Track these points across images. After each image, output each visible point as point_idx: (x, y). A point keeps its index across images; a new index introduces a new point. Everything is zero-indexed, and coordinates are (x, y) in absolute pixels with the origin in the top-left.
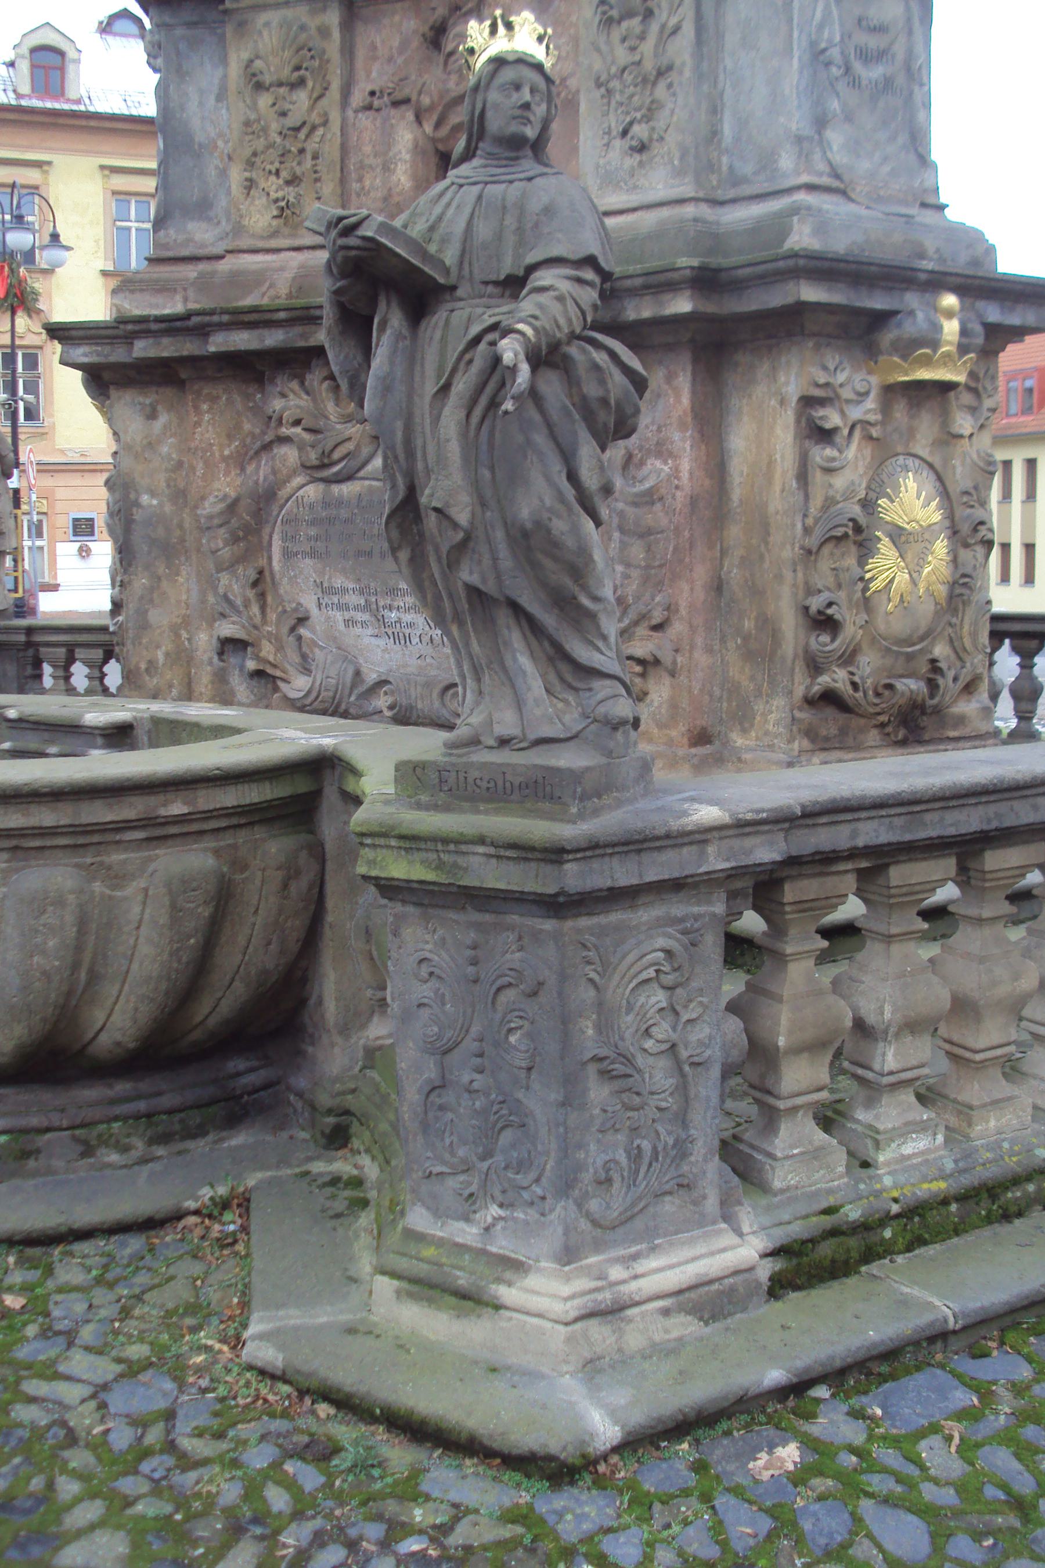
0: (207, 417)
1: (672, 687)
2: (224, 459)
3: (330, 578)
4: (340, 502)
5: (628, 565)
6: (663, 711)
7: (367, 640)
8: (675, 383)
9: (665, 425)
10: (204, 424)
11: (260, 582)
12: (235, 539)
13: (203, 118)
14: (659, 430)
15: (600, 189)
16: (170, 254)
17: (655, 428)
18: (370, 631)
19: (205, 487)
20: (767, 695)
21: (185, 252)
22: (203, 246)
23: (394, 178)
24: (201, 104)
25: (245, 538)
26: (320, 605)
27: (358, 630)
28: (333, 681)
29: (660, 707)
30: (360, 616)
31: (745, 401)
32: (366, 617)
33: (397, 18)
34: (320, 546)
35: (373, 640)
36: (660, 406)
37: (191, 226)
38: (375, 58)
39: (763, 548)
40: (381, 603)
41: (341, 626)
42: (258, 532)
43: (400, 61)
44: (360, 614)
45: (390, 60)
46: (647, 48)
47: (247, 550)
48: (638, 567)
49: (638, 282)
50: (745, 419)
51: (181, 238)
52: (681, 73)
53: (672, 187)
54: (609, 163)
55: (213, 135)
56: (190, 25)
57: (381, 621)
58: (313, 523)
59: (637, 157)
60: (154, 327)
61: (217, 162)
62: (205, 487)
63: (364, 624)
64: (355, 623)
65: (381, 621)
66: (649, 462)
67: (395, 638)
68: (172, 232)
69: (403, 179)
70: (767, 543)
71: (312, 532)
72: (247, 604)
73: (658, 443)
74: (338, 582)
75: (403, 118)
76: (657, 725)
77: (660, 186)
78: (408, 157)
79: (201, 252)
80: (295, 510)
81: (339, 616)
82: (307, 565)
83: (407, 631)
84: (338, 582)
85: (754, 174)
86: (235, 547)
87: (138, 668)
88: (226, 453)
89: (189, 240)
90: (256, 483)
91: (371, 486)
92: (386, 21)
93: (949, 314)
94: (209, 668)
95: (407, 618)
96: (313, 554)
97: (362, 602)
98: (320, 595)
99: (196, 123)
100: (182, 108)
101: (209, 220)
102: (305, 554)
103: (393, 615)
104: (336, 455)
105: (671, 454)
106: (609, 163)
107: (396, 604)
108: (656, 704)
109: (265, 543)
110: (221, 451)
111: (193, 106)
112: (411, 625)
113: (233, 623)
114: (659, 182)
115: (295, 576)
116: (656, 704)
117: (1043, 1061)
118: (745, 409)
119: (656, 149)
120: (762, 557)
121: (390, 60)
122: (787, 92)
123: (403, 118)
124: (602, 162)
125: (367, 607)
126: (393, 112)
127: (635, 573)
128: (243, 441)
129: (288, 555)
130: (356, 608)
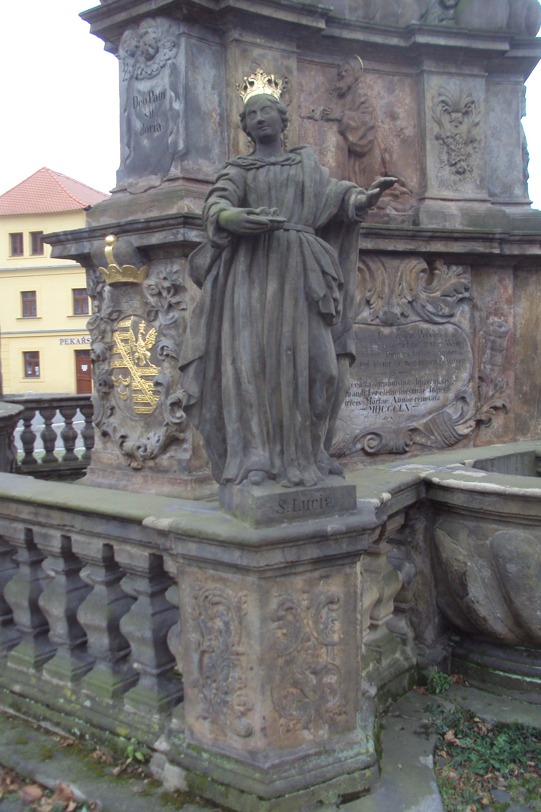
1: (505, 419)
5: (493, 365)
6: (500, 430)
7: (356, 412)
8: (504, 283)
13: (205, 97)
14: (496, 303)
15: (439, 187)
16: (192, 176)
17: (493, 303)
18: (361, 406)
20: (537, 417)
21: (200, 177)
22: (207, 175)
23: (326, 159)
24: (204, 88)
29: (498, 428)
30: (356, 399)
31: (523, 292)
32: (360, 399)
33: (313, 73)
35: (362, 412)
36: (496, 293)
37: (200, 161)
38: (303, 91)
39: (534, 355)
40: (372, 391)
43: (315, 96)
44: (357, 398)
45: (310, 94)
46: (464, 128)
48: (499, 366)
49: (518, 238)
50: (523, 300)
51: (196, 167)
52: (480, 143)
53: (476, 193)
54: (443, 176)
55: (210, 108)
56: (201, 39)
57: (368, 399)
59: (459, 177)
60: (171, 222)
61: (213, 125)
63: (358, 403)
65: (368, 399)
66: (491, 318)
67: (374, 409)
68: (191, 163)
69: (331, 160)
70: (536, 354)
73: (495, 309)
75: (331, 128)
77: (470, 192)
78: (333, 149)
79: (206, 178)
83: (382, 405)
85: (501, 193)
87: (199, 445)
89: (200, 170)
91: (360, 328)
92: (307, 73)
93: (109, 244)
95: (384, 398)
97: (360, 391)
99: (202, 99)
100: (195, 88)
101: (209, 159)
105: (503, 315)
106: (443, 176)
107: (379, 391)
108: (496, 427)
111: (200, 88)
112: (385, 402)
114: (469, 190)
116: (496, 427)
118: (523, 296)
119: (468, 174)
120: (533, 359)
121: (310, 94)
122: (518, 162)
123: (331, 128)
124: (439, 174)
126: (325, 124)
127: (497, 369)
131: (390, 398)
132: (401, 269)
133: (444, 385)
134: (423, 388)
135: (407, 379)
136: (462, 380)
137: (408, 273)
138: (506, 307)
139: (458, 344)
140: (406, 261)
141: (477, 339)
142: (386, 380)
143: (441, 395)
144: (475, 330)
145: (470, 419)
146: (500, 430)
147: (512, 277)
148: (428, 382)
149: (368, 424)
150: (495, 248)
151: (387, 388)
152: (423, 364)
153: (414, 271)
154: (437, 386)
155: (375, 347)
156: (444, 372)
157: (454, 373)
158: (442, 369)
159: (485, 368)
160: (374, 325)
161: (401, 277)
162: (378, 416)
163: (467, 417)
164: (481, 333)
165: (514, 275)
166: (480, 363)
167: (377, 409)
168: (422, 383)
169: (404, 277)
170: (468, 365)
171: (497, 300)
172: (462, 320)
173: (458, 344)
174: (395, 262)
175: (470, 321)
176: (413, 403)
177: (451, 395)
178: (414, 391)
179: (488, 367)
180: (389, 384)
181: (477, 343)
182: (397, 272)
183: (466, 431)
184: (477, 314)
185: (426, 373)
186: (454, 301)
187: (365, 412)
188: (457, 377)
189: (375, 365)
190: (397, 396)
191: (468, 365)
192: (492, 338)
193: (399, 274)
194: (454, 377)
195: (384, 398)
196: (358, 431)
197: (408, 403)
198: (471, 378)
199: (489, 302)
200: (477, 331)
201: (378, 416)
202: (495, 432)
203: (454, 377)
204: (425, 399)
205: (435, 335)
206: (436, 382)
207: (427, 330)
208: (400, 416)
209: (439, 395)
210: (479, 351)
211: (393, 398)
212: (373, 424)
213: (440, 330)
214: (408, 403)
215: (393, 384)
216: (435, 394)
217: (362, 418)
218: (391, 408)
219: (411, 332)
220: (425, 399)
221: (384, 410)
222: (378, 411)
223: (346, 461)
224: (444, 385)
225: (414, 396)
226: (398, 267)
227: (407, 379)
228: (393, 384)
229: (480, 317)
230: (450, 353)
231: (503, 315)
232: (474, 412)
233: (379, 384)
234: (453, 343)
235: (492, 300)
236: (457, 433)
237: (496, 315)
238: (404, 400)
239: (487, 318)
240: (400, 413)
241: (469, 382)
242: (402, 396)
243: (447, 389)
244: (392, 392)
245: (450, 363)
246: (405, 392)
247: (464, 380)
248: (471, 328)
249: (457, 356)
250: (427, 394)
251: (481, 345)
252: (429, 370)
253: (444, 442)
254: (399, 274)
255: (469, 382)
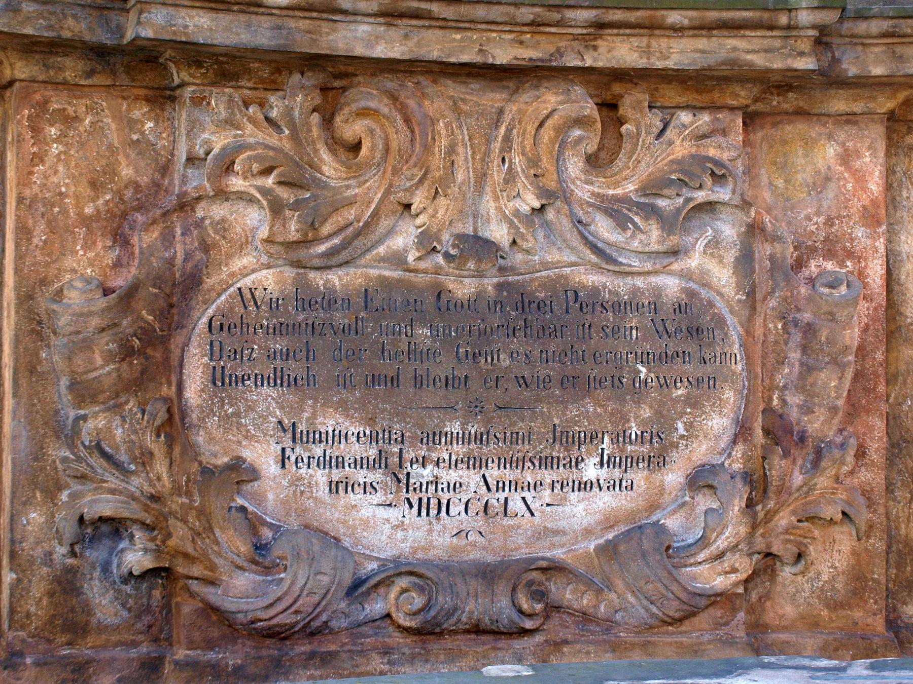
0: (55, 149)
2: (85, 221)
3: (314, 416)
4: (330, 300)
9: (839, 217)
10: (50, 160)
11: (174, 424)
12: (126, 352)
14: (829, 222)
17: (821, 220)
18: (379, 497)
19: (47, 264)
25: (141, 352)
26: (283, 461)
27: (355, 498)
28: (325, 579)
29: (833, 579)
30: (362, 476)
32: (375, 476)
34: (295, 368)
35: (382, 513)
40: (409, 454)
41: (323, 492)
42: (164, 341)
44: (364, 472)
47: (143, 372)
58: (279, 330)
62: (47, 264)
64: (348, 485)
65: (400, 479)
66: (813, 263)
67: (422, 507)
71: (279, 345)
72: (145, 458)
73: (827, 239)
74: (329, 423)
76: (828, 606)
80: (239, 309)
81: (321, 476)
82: (267, 399)
84: (329, 423)
86: (125, 366)
88: (89, 210)
90: (171, 262)
94: (45, 569)
95: (452, 476)
96: (279, 379)
97: (373, 452)
98: (288, 443)
102: (261, 380)
103: (428, 473)
104: (326, 229)
107: (434, 456)
109: (175, 362)
110: (79, 207)
112: (455, 487)
113: (113, 492)
115: (237, 414)
116: (825, 577)
117: (3, 655)
125: (381, 461)
128: (119, 194)
129: (219, 380)
130: (358, 463)
131: (472, 479)
132: (507, 117)
133: (645, 449)
134: (575, 453)
135: (521, 427)
136: (712, 433)
137: (531, 129)
138: (860, 232)
139: (694, 332)
140: (526, 96)
141: (759, 321)
142: (455, 427)
143: (639, 476)
144: (751, 294)
145: (734, 548)
146: (839, 586)
147: (881, 146)
148: (594, 437)
149: (406, 547)
150: (801, 54)
151: (459, 449)
152: (576, 385)
153: (549, 123)
154: (622, 451)
155: (423, 332)
156: (646, 412)
157: (681, 415)
158: (638, 403)
159: (783, 402)
160: (425, 272)
161: (507, 139)
162: (437, 527)
163: (722, 543)
164: (773, 303)
165: (889, 138)
166: (771, 389)
167: (431, 507)
168: (570, 443)
169: (516, 140)
170: (729, 395)
171: (833, 214)
172: (712, 266)
173: (694, 332)
174: (492, 98)
175: (735, 267)
176: (546, 495)
177: (673, 477)
178: (547, 462)
179: (795, 400)
180: (465, 439)
181: (759, 332)
182: (497, 124)
183: (720, 582)
184: (763, 250)
185: (586, 412)
186: (679, 210)
187: (393, 514)
188: (689, 426)
189: (418, 382)
190: (494, 473)
191: (729, 395)
192: (807, 316)
193: (502, 130)
194: (680, 425)
195: (452, 476)
196: (374, 566)
197: (526, 494)
198: (742, 432)
199: (808, 218)
200: (759, 296)
201: (437, 527)
202: (822, 589)
203: (680, 425)
204: (583, 486)
205: (620, 307)
206: (620, 437)
207: (595, 291)
208: (507, 531)
209: (630, 475)
210: (764, 356)
211: (478, 478)
212: (424, 549)
213: (635, 291)
214: (528, 496)
215: (479, 438)
216: (617, 473)
217: (387, 528)
218: (479, 506)
219: (541, 295)
220: (583, 486)
221: (453, 511)
222: (433, 512)
223: (333, 648)
224: (645, 449)
225: (548, 476)
226: (501, 112)
227: (521, 427)
228: (479, 438)
229: (772, 258)
230: (665, 358)
231: (850, 254)
232: (743, 530)
233: (433, 437)
234: (678, 330)
235: (818, 214)
236: (685, 589)
237: (830, 254)
238: (515, 485)
239: (799, 264)
240: (507, 521)
241: (734, 442)
242: (509, 474)
243: (657, 462)
244: (475, 462)
245: (664, 385)
246: (519, 463)
247: (718, 437)
248: (739, 287)
249: (688, 367)
250: (591, 471)
251: (771, 338)
252: (597, 403)
253: (647, 610)
254: (502, 130)
255: (734, 442)
